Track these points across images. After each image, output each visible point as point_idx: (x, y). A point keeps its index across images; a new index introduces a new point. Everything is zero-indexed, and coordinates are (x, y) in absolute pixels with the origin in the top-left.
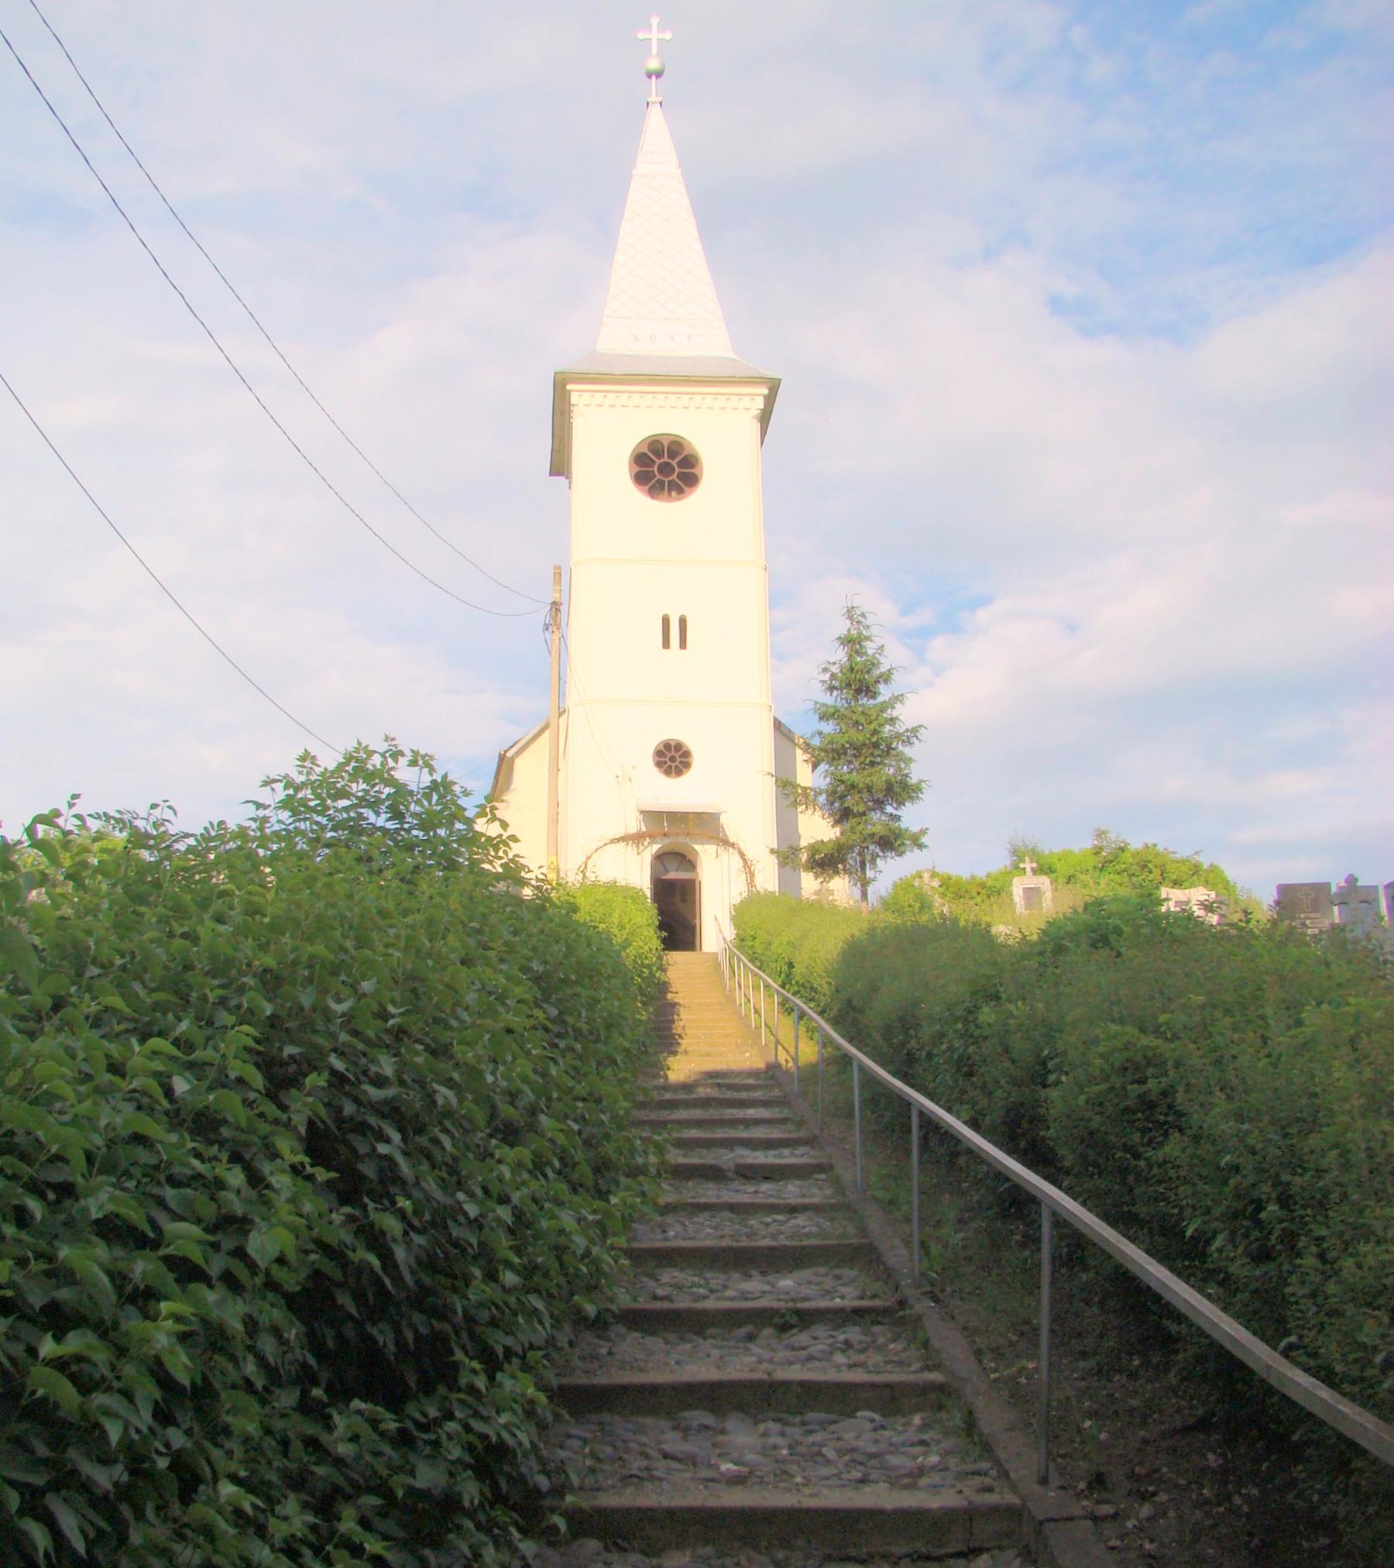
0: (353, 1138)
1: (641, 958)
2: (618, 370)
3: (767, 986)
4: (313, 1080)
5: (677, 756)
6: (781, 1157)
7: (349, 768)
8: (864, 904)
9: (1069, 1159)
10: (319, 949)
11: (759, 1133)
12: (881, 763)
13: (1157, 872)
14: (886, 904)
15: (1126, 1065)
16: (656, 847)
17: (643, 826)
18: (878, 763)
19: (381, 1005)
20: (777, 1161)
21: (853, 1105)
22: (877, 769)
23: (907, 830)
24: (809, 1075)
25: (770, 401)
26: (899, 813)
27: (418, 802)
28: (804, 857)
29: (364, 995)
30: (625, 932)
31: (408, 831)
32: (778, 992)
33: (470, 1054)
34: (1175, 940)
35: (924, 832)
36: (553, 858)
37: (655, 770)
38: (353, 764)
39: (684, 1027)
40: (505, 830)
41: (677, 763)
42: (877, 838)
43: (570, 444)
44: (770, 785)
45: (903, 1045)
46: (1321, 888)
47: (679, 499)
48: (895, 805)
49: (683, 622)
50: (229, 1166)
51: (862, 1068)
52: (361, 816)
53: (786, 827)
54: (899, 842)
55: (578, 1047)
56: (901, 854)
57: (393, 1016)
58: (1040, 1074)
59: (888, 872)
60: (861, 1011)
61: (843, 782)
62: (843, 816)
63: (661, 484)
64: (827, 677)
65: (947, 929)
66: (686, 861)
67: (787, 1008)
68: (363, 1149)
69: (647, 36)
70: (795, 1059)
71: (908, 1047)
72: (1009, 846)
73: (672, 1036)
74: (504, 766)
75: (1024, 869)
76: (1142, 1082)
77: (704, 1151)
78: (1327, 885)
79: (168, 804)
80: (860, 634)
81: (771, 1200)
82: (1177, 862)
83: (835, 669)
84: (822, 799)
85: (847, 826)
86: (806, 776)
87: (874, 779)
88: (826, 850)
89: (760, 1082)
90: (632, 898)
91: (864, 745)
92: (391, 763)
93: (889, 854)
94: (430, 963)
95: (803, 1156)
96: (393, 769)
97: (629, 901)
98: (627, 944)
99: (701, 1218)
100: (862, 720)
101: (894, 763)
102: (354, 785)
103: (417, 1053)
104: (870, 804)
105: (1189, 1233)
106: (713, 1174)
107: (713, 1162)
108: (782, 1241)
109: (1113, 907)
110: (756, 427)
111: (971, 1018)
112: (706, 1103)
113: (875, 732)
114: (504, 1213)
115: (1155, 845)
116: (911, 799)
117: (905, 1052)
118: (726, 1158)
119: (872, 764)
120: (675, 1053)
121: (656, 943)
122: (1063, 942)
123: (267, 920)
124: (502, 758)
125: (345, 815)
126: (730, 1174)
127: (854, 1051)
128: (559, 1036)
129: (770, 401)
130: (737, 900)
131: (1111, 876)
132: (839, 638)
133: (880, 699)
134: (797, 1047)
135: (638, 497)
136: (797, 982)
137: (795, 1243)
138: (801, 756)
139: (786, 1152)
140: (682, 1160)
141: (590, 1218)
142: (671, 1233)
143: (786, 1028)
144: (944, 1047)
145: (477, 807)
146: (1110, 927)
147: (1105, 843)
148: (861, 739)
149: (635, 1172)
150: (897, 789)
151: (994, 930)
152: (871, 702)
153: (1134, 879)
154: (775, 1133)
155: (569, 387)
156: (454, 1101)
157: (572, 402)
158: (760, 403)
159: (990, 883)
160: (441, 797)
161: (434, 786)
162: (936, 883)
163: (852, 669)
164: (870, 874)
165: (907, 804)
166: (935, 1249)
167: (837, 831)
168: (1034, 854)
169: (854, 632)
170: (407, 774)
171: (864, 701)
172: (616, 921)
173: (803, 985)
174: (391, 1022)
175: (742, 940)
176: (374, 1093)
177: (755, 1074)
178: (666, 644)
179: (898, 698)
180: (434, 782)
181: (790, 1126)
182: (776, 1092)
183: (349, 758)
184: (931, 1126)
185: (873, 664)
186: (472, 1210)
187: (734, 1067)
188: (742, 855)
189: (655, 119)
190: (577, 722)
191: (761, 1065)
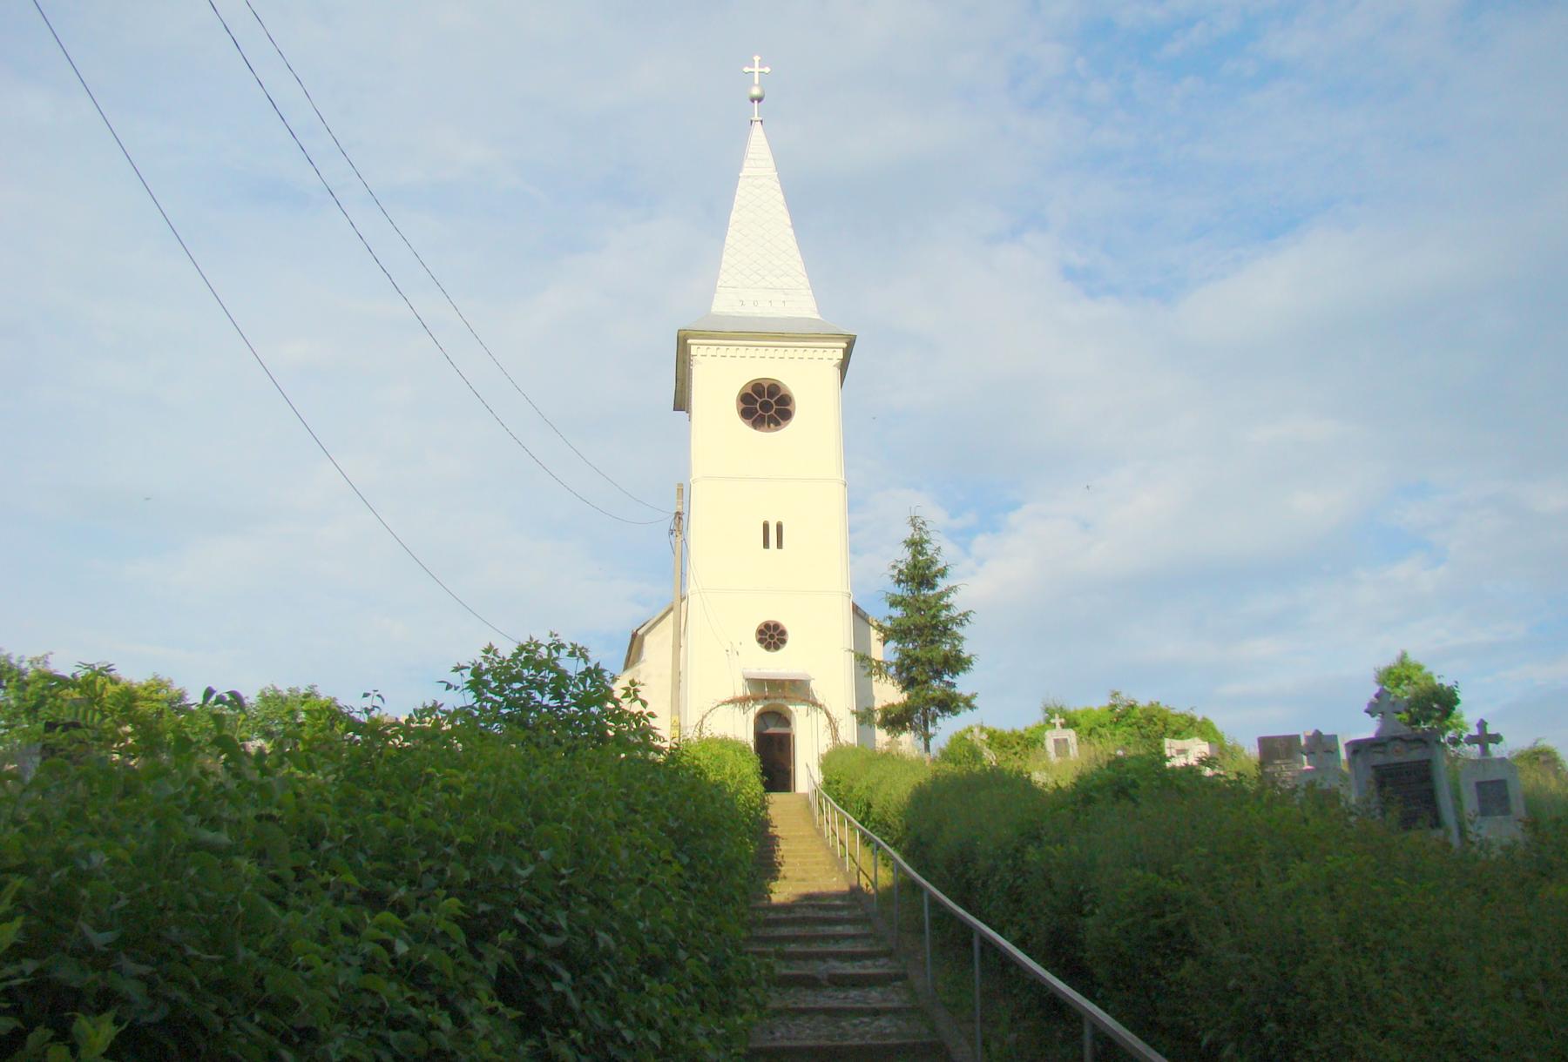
0: (532, 978)
1: (748, 801)
2: (728, 328)
3: (849, 821)
4: (505, 936)
5: (775, 634)
6: (865, 967)
7: (521, 658)
8: (927, 754)
9: (1101, 972)
10: (506, 824)
11: (845, 947)
12: (940, 641)
13: (1160, 724)
14: (946, 755)
15: (1148, 901)
16: (759, 708)
17: (748, 690)
18: (937, 642)
20: (862, 971)
21: (924, 923)
22: (936, 645)
23: (960, 695)
24: (885, 896)
25: (848, 353)
26: (954, 681)
27: (576, 686)
28: (878, 717)
31: (567, 708)
32: (860, 829)
34: (1180, 790)
35: (974, 696)
36: (676, 718)
37: (757, 645)
38: (525, 654)
39: (783, 856)
40: (645, 708)
41: (775, 640)
42: (936, 702)
43: (690, 387)
46: (1291, 741)
47: (777, 430)
48: (951, 674)
49: (779, 527)
50: (440, 1012)
51: (931, 895)
52: (530, 697)
53: (863, 692)
54: (954, 705)
57: (563, 877)
58: (1077, 905)
59: (946, 728)
61: (909, 656)
62: (909, 683)
63: (762, 418)
65: (996, 778)
66: (784, 719)
67: (866, 841)
68: (540, 986)
69: (752, 70)
70: (874, 884)
72: (1042, 706)
74: (636, 643)
75: (1055, 724)
76: (1163, 915)
77: (802, 963)
78: (1297, 737)
79: (377, 693)
80: (921, 538)
81: (859, 1005)
82: (1177, 716)
83: (902, 566)
84: (893, 670)
85: (913, 691)
86: (879, 651)
87: (934, 654)
89: (845, 903)
90: (740, 751)
91: (926, 627)
92: (555, 654)
93: (946, 714)
95: (882, 966)
96: (556, 658)
97: (738, 754)
98: (738, 792)
99: (802, 1020)
100: (923, 606)
101: (949, 641)
102: (525, 671)
104: (931, 674)
105: (1204, 1042)
106: (811, 983)
107: (809, 973)
108: (869, 1040)
109: (1130, 764)
110: (837, 373)
111: (1019, 855)
112: (804, 921)
113: (934, 617)
114: (654, 1037)
115: (1158, 703)
116: (964, 669)
117: (964, 881)
118: (819, 969)
119: (932, 642)
120: (776, 879)
121: (760, 788)
122: (1092, 794)
123: (461, 797)
124: (634, 636)
125: (517, 695)
126: (825, 983)
127: (924, 881)
128: (692, 879)
129: (848, 353)
131: (1124, 728)
132: (905, 542)
133: (938, 590)
134: (876, 875)
135: (744, 428)
136: (874, 819)
137: (879, 1042)
138: (875, 635)
139: (869, 963)
140: (785, 971)
141: (719, 1032)
142: (778, 1034)
143: (864, 857)
144: (997, 878)
145: (623, 689)
146: (1129, 780)
147: (1118, 702)
148: (923, 621)
149: (748, 984)
151: (1033, 778)
152: (931, 592)
153: (1143, 731)
154: (860, 947)
155: (689, 341)
156: (612, 945)
157: (692, 353)
159: (1027, 736)
160: (593, 681)
161: (588, 672)
162: (984, 736)
163: (915, 566)
164: (931, 730)
165: (961, 673)
166: (994, 1046)
167: (905, 695)
168: (1062, 712)
169: (917, 537)
170: (572, 667)
171: (926, 592)
172: (728, 773)
173: (879, 822)
174: (563, 882)
176: (549, 940)
177: (838, 895)
179: (951, 589)
180: (588, 669)
181: (871, 941)
182: (859, 912)
183: (522, 648)
184: (987, 943)
185: (932, 562)
186: (628, 1035)
187: (824, 890)
188: (828, 714)
189: (758, 132)
190: (696, 608)
191: (846, 888)
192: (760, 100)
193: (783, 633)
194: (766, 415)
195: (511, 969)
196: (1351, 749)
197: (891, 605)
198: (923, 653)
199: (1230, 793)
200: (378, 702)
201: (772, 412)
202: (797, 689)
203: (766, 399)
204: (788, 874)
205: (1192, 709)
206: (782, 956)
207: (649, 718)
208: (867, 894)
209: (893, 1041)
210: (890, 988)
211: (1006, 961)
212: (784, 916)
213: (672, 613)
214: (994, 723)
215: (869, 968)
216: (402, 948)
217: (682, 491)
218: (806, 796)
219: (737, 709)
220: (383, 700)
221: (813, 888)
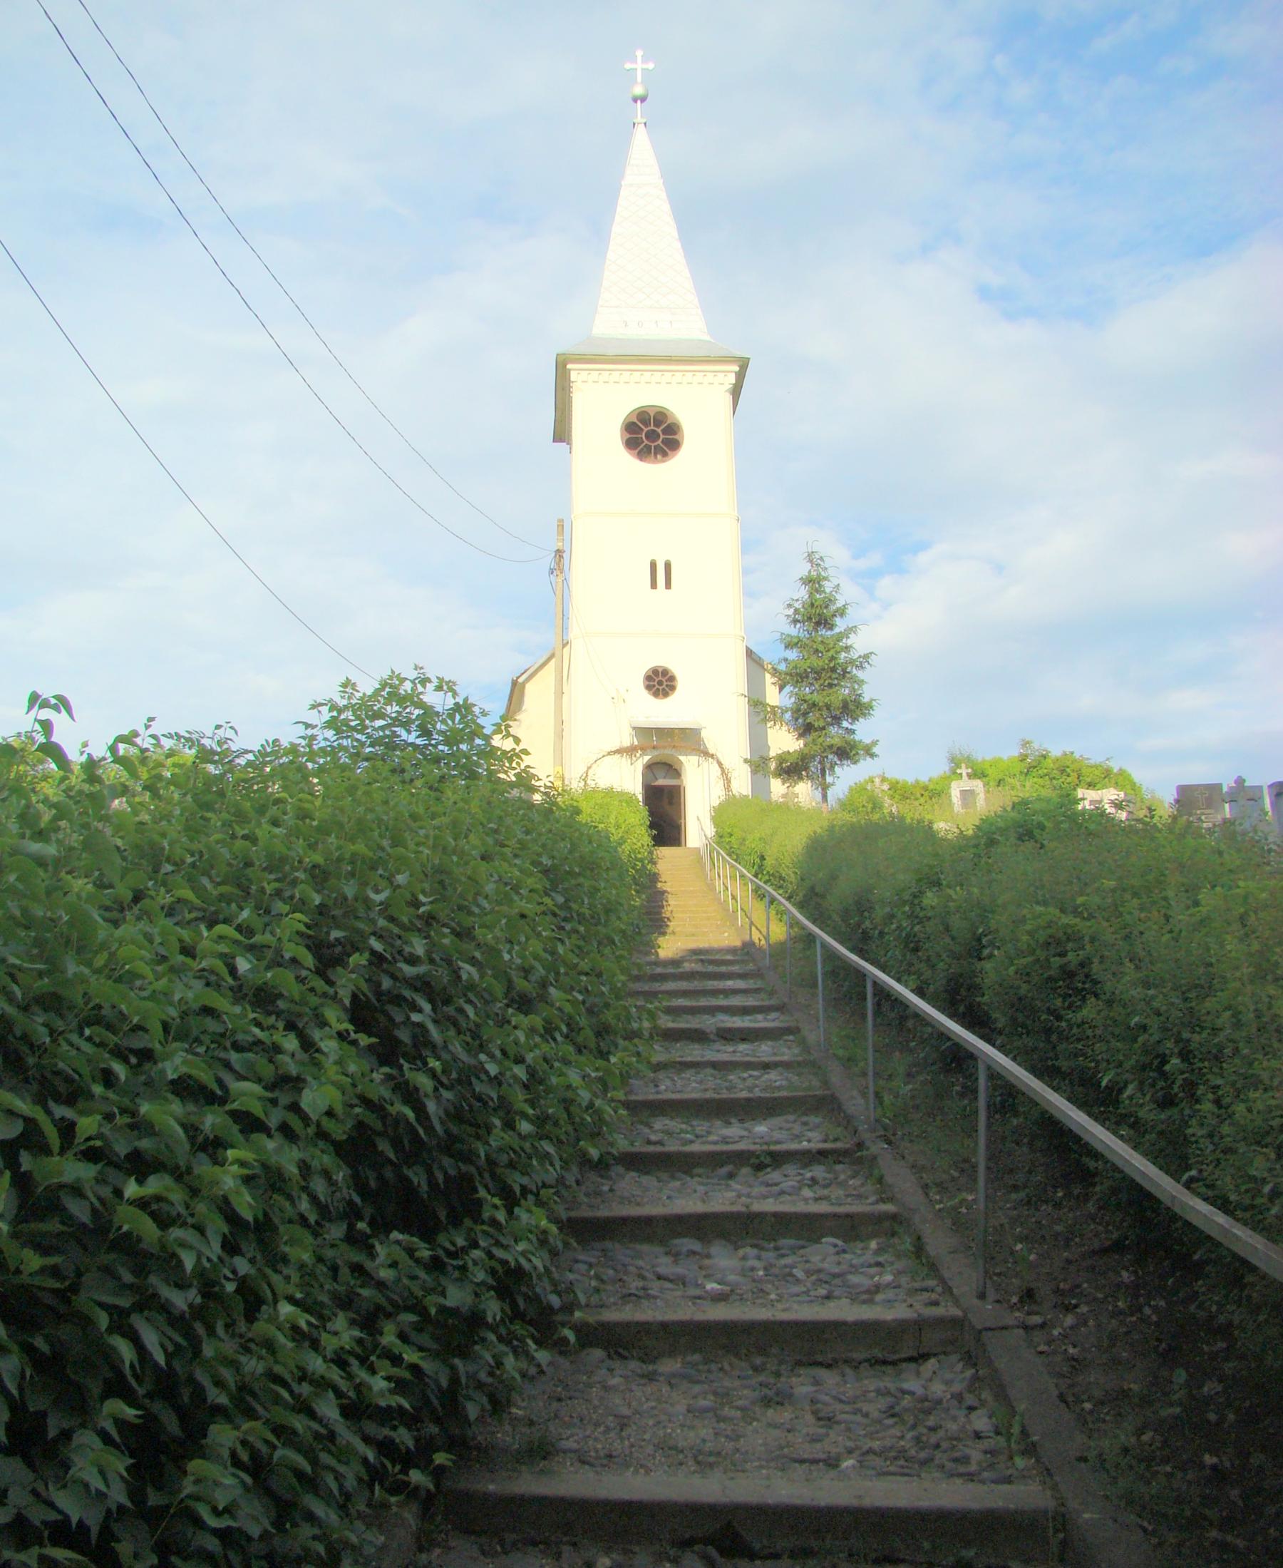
0: (389, 1007)
1: (634, 853)
2: (611, 352)
3: (742, 876)
6: (755, 1021)
8: (825, 805)
9: (1001, 1020)
10: (360, 847)
11: (736, 1001)
14: (844, 805)
15: (1050, 940)
16: (647, 758)
18: (836, 685)
19: (413, 895)
22: (834, 690)
23: (860, 742)
24: (778, 951)
25: (740, 377)
26: (853, 727)
27: (443, 721)
28: (773, 765)
29: (399, 886)
30: (621, 831)
31: (435, 746)
32: (752, 881)
33: (490, 936)
34: (1090, 834)
35: (875, 743)
38: (388, 690)
42: (835, 749)
44: (743, 705)
45: (859, 925)
49: (668, 566)
51: (824, 946)
53: (757, 739)
54: (853, 752)
55: (582, 929)
56: (855, 763)
57: (424, 904)
58: (976, 948)
59: (845, 778)
60: (823, 896)
61: (805, 701)
62: (806, 730)
63: (648, 448)
64: (791, 611)
65: (896, 826)
66: (673, 769)
67: (759, 894)
68: (399, 1018)
70: (767, 938)
71: (863, 926)
73: (662, 920)
75: (961, 774)
78: (1220, 785)
80: (819, 575)
82: (1091, 767)
83: (798, 605)
84: (788, 716)
85: (809, 738)
86: (773, 696)
87: (832, 698)
88: (792, 760)
89: (737, 958)
91: (823, 669)
92: (420, 688)
93: (845, 762)
94: (455, 858)
95: (774, 1020)
96: (421, 693)
97: (624, 804)
98: (622, 841)
99: (688, 1074)
100: (821, 648)
102: (389, 708)
103: (444, 936)
105: (1104, 1083)
106: (698, 1036)
107: (698, 1026)
108: (757, 1093)
109: (1037, 806)
110: (729, 398)
112: (691, 976)
113: (832, 659)
114: (520, 1071)
116: (864, 715)
118: (708, 1023)
119: (830, 686)
120: (664, 934)
121: (647, 840)
123: (315, 823)
124: (514, 683)
126: (712, 1037)
128: (565, 919)
129: (740, 377)
130: (716, 803)
131: (1035, 780)
133: (837, 630)
134: (768, 928)
135: (628, 460)
137: (768, 1095)
138: (769, 679)
139: (760, 1017)
140: (671, 1025)
141: (593, 1075)
143: (759, 911)
144: (894, 926)
148: (820, 664)
149: (632, 1035)
150: (852, 707)
151: (935, 827)
152: (829, 633)
153: (1055, 782)
154: (750, 1001)
155: (569, 366)
156: (476, 975)
158: (732, 379)
159: (931, 787)
160: (463, 717)
161: (457, 707)
162: (885, 787)
163: (812, 605)
164: (829, 779)
165: (860, 720)
166: (888, 1099)
167: (801, 743)
168: (969, 761)
169: (814, 573)
170: (432, 697)
171: (823, 632)
173: (773, 875)
175: (721, 837)
176: (408, 970)
177: (733, 951)
178: (654, 585)
179: (852, 630)
180: (457, 704)
181: (763, 995)
182: (751, 966)
183: (384, 685)
184: (883, 994)
186: (493, 1069)
187: (715, 945)
188: (720, 764)
190: (579, 655)
191: (738, 943)
192: (643, 99)
193: (672, 679)
194: (653, 445)
195: (364, 995)
196: (1274, 791)
197: (786, 647)
198: (820, 697)
199: (1144, 830)
200: (231, 734)
201: (659, 442)
202: (689, 739)
203: (652, 427)
204: (678, 929)
205: (1108, 759)
206: (669, 1011)
207: (523, 756)
208: (760, 949)
209: (784, 1093)
210: (781, 1042)
211: (898, 1003)
212: (672, 971)
213: (554, 660)
214: (893, 774)
215: (759, 1022)
216: (243, 965)
217: (561, 527)
218: (698, 850)
219: (624, 759)
220: (236, 733)
221: (703, 944)
